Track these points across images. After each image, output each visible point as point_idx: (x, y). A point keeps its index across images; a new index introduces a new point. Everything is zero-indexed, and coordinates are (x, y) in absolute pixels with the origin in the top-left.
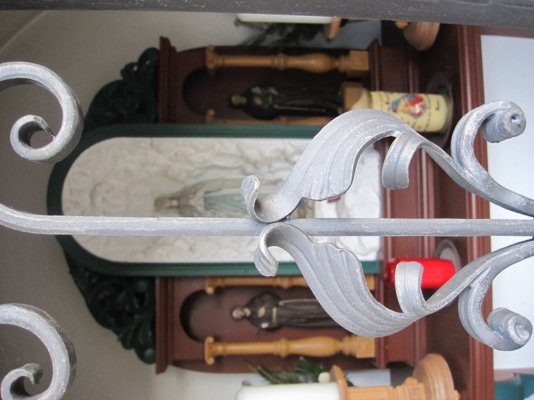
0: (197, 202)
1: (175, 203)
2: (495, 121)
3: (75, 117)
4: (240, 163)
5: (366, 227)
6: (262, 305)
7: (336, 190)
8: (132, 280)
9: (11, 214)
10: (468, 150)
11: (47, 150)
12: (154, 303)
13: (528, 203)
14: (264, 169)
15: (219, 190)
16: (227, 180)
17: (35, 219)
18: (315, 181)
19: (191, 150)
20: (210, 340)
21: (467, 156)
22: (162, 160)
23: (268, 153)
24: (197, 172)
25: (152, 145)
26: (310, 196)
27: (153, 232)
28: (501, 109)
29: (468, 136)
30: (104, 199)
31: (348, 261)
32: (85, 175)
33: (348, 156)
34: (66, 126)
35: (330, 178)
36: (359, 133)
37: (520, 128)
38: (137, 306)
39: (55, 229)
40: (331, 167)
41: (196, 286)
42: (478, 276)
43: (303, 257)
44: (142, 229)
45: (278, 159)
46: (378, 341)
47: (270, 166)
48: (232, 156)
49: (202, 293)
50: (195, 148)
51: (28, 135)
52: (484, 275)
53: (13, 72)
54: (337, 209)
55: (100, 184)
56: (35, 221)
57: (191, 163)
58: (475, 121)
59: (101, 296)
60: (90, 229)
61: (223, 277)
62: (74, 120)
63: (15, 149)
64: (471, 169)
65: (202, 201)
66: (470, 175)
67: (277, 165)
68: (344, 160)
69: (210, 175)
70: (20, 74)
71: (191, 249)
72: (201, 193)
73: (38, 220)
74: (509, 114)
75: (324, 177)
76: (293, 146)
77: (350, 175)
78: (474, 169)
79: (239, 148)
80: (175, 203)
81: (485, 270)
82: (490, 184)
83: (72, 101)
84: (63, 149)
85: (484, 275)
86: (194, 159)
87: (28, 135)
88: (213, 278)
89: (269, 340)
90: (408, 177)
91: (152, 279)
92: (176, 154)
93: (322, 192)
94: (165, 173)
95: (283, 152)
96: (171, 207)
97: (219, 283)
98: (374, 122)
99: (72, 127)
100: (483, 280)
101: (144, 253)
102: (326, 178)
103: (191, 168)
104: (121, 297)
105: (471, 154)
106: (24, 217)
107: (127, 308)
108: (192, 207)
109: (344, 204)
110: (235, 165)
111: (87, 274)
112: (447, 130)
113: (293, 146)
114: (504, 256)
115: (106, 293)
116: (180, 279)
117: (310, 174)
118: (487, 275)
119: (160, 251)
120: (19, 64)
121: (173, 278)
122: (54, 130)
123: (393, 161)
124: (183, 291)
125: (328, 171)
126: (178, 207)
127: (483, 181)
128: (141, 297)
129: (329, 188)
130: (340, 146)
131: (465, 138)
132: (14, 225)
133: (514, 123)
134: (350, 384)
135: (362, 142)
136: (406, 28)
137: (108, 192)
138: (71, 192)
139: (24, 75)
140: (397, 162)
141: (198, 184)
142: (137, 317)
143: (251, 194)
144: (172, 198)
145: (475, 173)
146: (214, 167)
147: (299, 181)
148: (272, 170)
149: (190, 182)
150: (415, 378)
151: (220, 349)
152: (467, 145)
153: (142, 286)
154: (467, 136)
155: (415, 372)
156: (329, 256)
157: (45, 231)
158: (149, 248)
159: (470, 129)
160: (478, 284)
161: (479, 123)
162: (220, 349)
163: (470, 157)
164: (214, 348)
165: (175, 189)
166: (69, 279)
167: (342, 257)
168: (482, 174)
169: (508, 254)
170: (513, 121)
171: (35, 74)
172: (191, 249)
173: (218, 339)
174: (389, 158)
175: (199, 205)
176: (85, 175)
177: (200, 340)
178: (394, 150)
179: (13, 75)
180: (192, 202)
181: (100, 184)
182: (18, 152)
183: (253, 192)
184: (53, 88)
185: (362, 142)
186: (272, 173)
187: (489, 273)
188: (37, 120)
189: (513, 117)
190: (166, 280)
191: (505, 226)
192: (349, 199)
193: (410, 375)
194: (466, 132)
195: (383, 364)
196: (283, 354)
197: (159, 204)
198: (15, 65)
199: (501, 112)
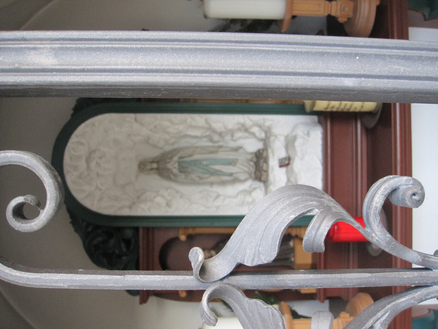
0: (173, 166)
1: (155, 166)
2: (400, 194)
3: (57, 197)
4: (208, 133)
5: (290, 282)
7: (264, 259)
8: (119, 229)
9: (9, 272)
10: (376, 217)
11: (35, 224)
12: (138, 248)
13: (423, 260)
14: (228, 138)
15: (191, 155)
16: (197, 147)
17: (29, 276)
18: (248, 251)
19: (168, 124)
21: (375, 223)
22: (145, 131)
23: (230, 126)
24: (173, 140)
25: (136, 120)
26: (244, 262)
27: (120, 287)
28: (404, 185)
29: (376, 207)
30: (97, 163)
31: (273, 316)
32: (82, 144)
33: (275, 232)
34: (49, 205)
35: (260, 249)
36: (285, 211)
38: (124, 250)
39: (44, 284)
40: (261, 240)
41: (171, 235)
42: (379, 318)
43: (238, 307)
44: (112, 285)
45: (239, 130)
46: (317, 289)
47: (232, 136)
48: (202, 128)
49: (177, 239)
50: (171, 121)
51: (20, 212)
52: (384, 317)
53: (6, 160)
54: (287, 172)
55: (94, 151)
56: (28, 278)
57: (168, 133)
58: (382, 195)
59: (95, 242)
60: (71, 284)
61: (194, 228)
62: (56, 200)
63: (10, 223)
64: (377, 233)
65: (176, 165)
66: (377, 238)
67: (239, 134)
68: (271, 236)
69: (183, 143)
70: (12, 162)
71: (168, 205)
72: (176, 158)
73: (31, 277)
74: (410, 192)
75: (256, 248)
76: (251, 120)
77: (276, 248)
78: (380, 233)
79: (207, 121)
80: (155, 166)
81: (385, 313)
82: (393, 245)
83: (54, 184)
84: (48, 223)
85: (384, 317)
86: (171, 130)
87: (20, 212)
88: (186, 228)
90: (323, 244)
91: (136, 229)
92: (155, 127)
93: (253, 260)
94: (147, 141)
95: (243, 125)
96: (152, 169)
97: (191, 231)
98: (298, 199)
99: (54, 205)
100: (384, 321)
101: (130, 207)
102: (257, 249)
103: (167, 137)
104: (112, 242)
105: (378, 221)
106: (20, 275)
107: (117, 252)
108: (169, 170)
109: (292, 170)
110: (204, 135)
111: (84, 224)
112: (378, 110)
113: (251, 120)
114: (402, 302)
115: (100, 239)
116: (159, 229)
117: (245, 244)
118: (387, 317)
119: (142, 206)
120: (11, 153)
121: (153, 228)
122: (41, 204)
123: (311, 237)
124: (161, 239)
125: (259, 243)
126: (157, 169)
127: (387, 243)
128: (128, 242)
129: (259, 257)
130: (269, 223)
131: (373, 208)
132: (12, 281)
133: (414, 199)
134: (295, 315)
135: (286, 220)
136: (346, 22)
137: (100, 158)
138: (71, 158)
139: (15, 162)
140: (314, 237)
141: (174, 150)
142: (124, 258)
143: (196, 265)
144: (152, 162)
145: (380, 236)
147: (236, 248)
148: (234, 138)
149: (168, 148)
150: (347, 312)
152: (375, 214)
153: (129, 233)
154: (375, 207)
155: (348, 307)
156: (258, 310)
157: (37, 285)
158: (134, 203)
159: (378, 201)
160: (379, 325)
161: (385, 196)
163: (377, 223)
165: (154, 153)
166: (70, 228)
167: (268, 312)
168: (386, 237)
169: (405, 300)
170: (414, 197)
171: (23, 161)
174: (309, 233)
175: (175, 168)
176: (82, 144)
178: (312, 227)
179: (6, 162)
180: (169, 166)
181: (94, 151)
182: (13, 226)
183: (198, 263)
184: (39, 173)
185: (286, 220)
186: (234, 141)
187: (388, 316)
188: (27, 200)
189: (414, 194)
190: (147, 229)
191: (403, 278)
192: (297, 165)
193: (344, 310)
194: (374, 204)
195: (322, 297)
197: (142, 167)
198: (7, 154)
199: (405, 187)
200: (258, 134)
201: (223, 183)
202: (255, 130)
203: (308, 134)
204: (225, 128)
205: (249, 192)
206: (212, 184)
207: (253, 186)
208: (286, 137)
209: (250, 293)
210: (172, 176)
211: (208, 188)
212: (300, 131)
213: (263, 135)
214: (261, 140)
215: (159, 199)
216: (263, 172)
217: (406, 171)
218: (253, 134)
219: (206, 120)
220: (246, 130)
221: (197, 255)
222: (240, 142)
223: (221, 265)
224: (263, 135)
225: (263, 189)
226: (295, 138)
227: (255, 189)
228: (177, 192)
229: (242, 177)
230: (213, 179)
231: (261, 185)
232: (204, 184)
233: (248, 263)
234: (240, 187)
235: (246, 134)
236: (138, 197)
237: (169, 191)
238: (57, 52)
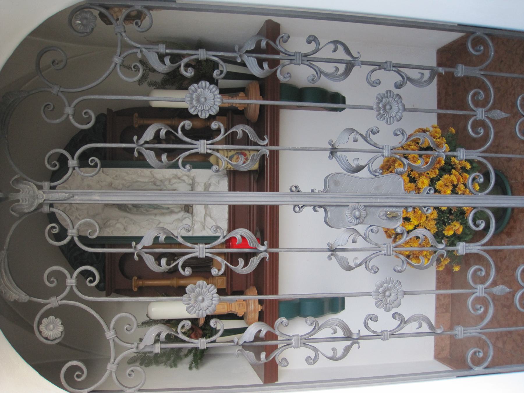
4: (153, 180)
6: (458, 264)
19: (125, 174)
20: (135, 278)
23: (167, 177)
37: (378, 132)
45: (174, 178)
47: (170, 182)
50: (127, 173)
57: (125, 180)
71: (125, 229)
86: (126, 178)
89: (168, 279)
92: (116, 176)
119: (107, 230)
146: (137, 181)
151: (141, 283)
162: (141, 283)
164: (137, 283)
172: (125, 229)
173: (140, 278)
177: (130, 278)
186: (171, 185)
196: (175, 286)
200: (187, 181)
201: (163, 214)
202: (185, 178)
203: (219, 183)
204: (164, 177)
205: (181, 220)
206: (156, 215)
207: (184, 216)
208: (205, 184)
209: (146, 253)
210: (128, 210)
211: (153, 217)
212: (214, 180)
213: (191, 182)
214: (190, 184)
215: (119, 225)
216: (190, 207)
217: (273, 208)
218: (184, 181)
219: (151, 172)
220: (179, 178)
221: (134, 244)
222: (176, 186)
223: (139, 247)
224: (191, 182)
225: (191, 218)
226: (210, 185)
227: (185, 218)
228: (131, 220)
229: (176, 210)
230: (156, 211)
231: (190, 215)
232: (150, 214)
233: (146, 245)
234: (175, 217)
235: (179, 181)
236: (104, 224)
237: (125, 219)
238: (100, 196)
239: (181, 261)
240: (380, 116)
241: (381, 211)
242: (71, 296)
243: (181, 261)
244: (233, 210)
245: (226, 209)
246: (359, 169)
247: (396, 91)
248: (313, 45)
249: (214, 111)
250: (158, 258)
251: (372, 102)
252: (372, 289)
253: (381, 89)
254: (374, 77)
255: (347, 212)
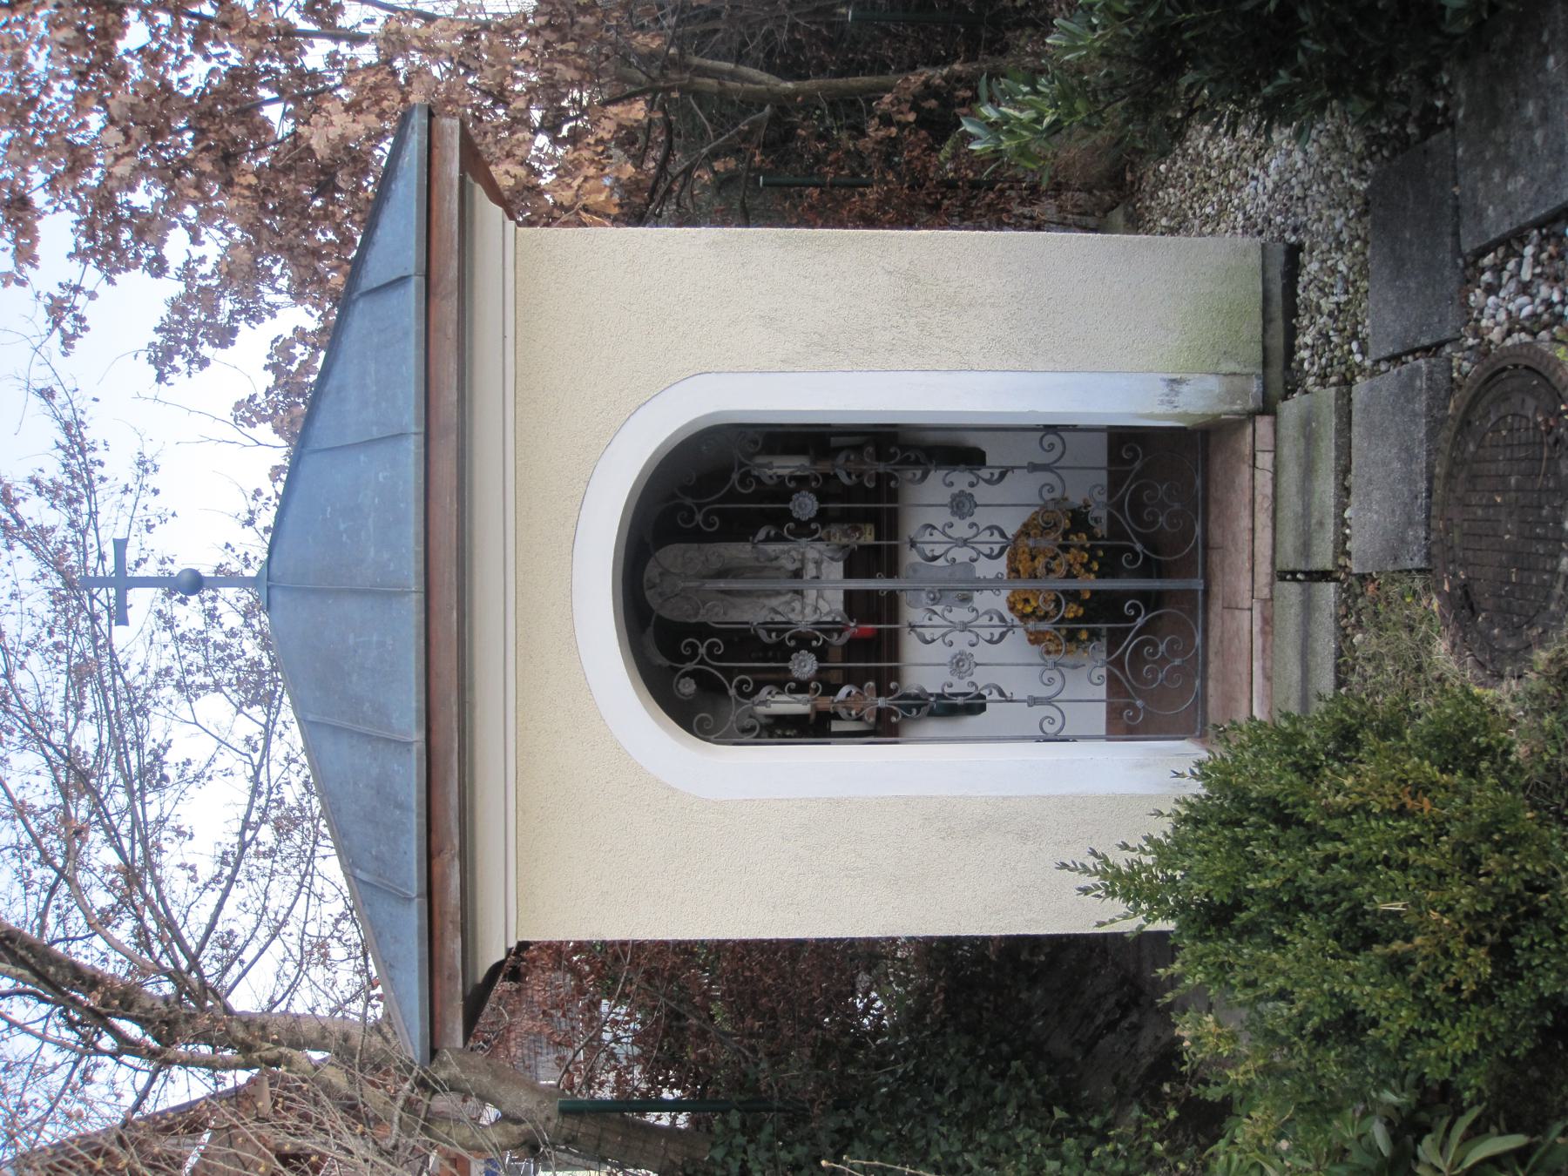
239: (787, 635)
240: (954, 513)
241: (954, 594)
242: (702, 662)
243: (787, 635)
244: (849, 595)
245: (841, 596)
246: (935, 558)
247: (969, 490)
248: (974, 530)
249: (812, 515)
250: (769, 631)
251: (947, 500)
252: (947, 660)
253: (955, 490)
254: (948, 480)
255: (923, 595)
